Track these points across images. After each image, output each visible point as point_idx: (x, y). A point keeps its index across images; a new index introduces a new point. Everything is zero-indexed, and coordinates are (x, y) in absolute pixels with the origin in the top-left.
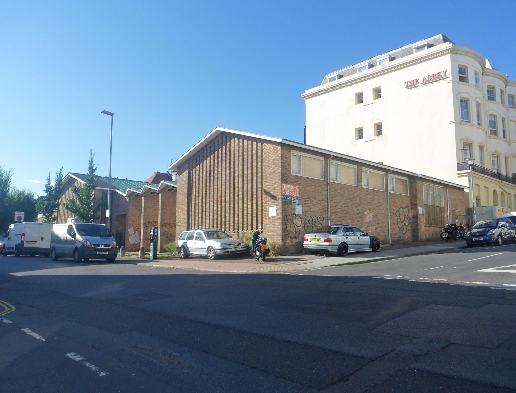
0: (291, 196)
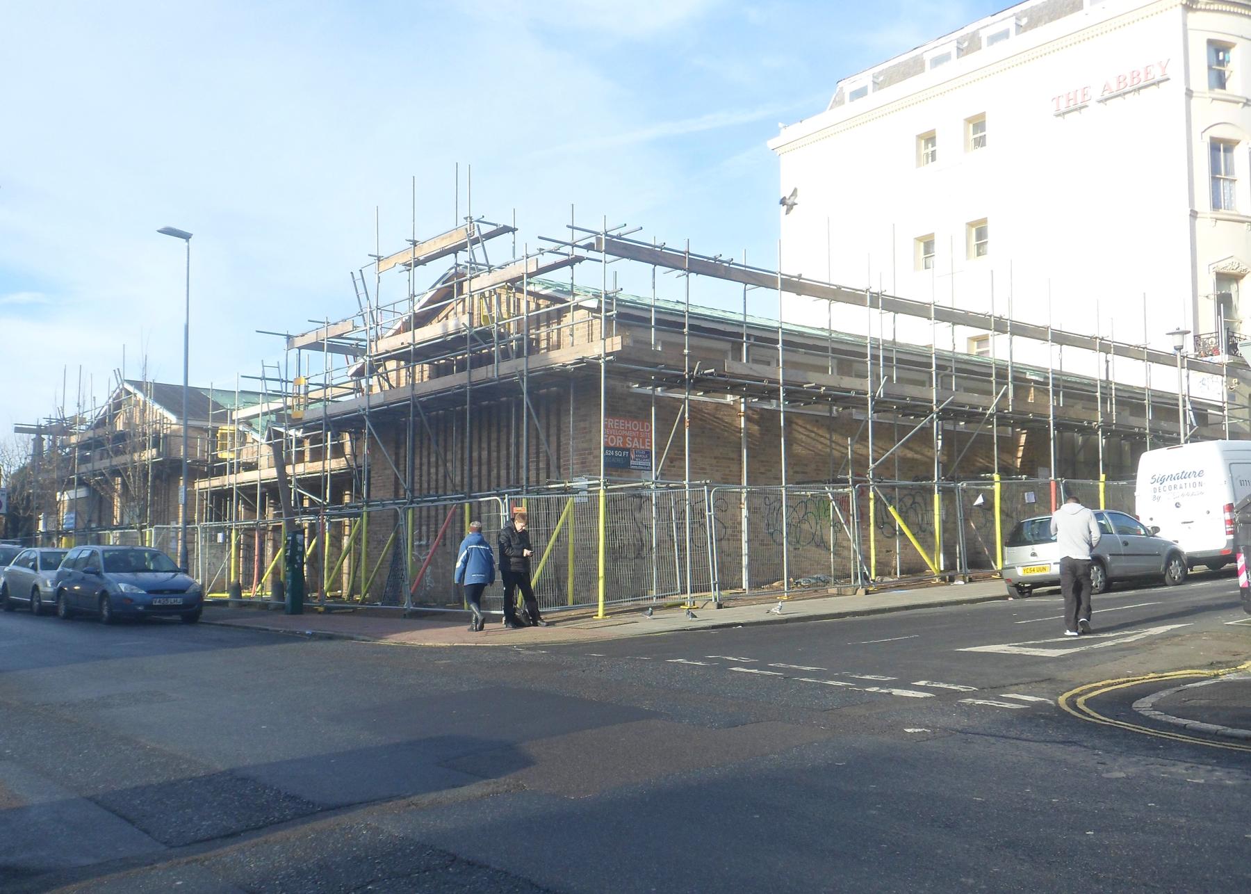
0: (628, 450)
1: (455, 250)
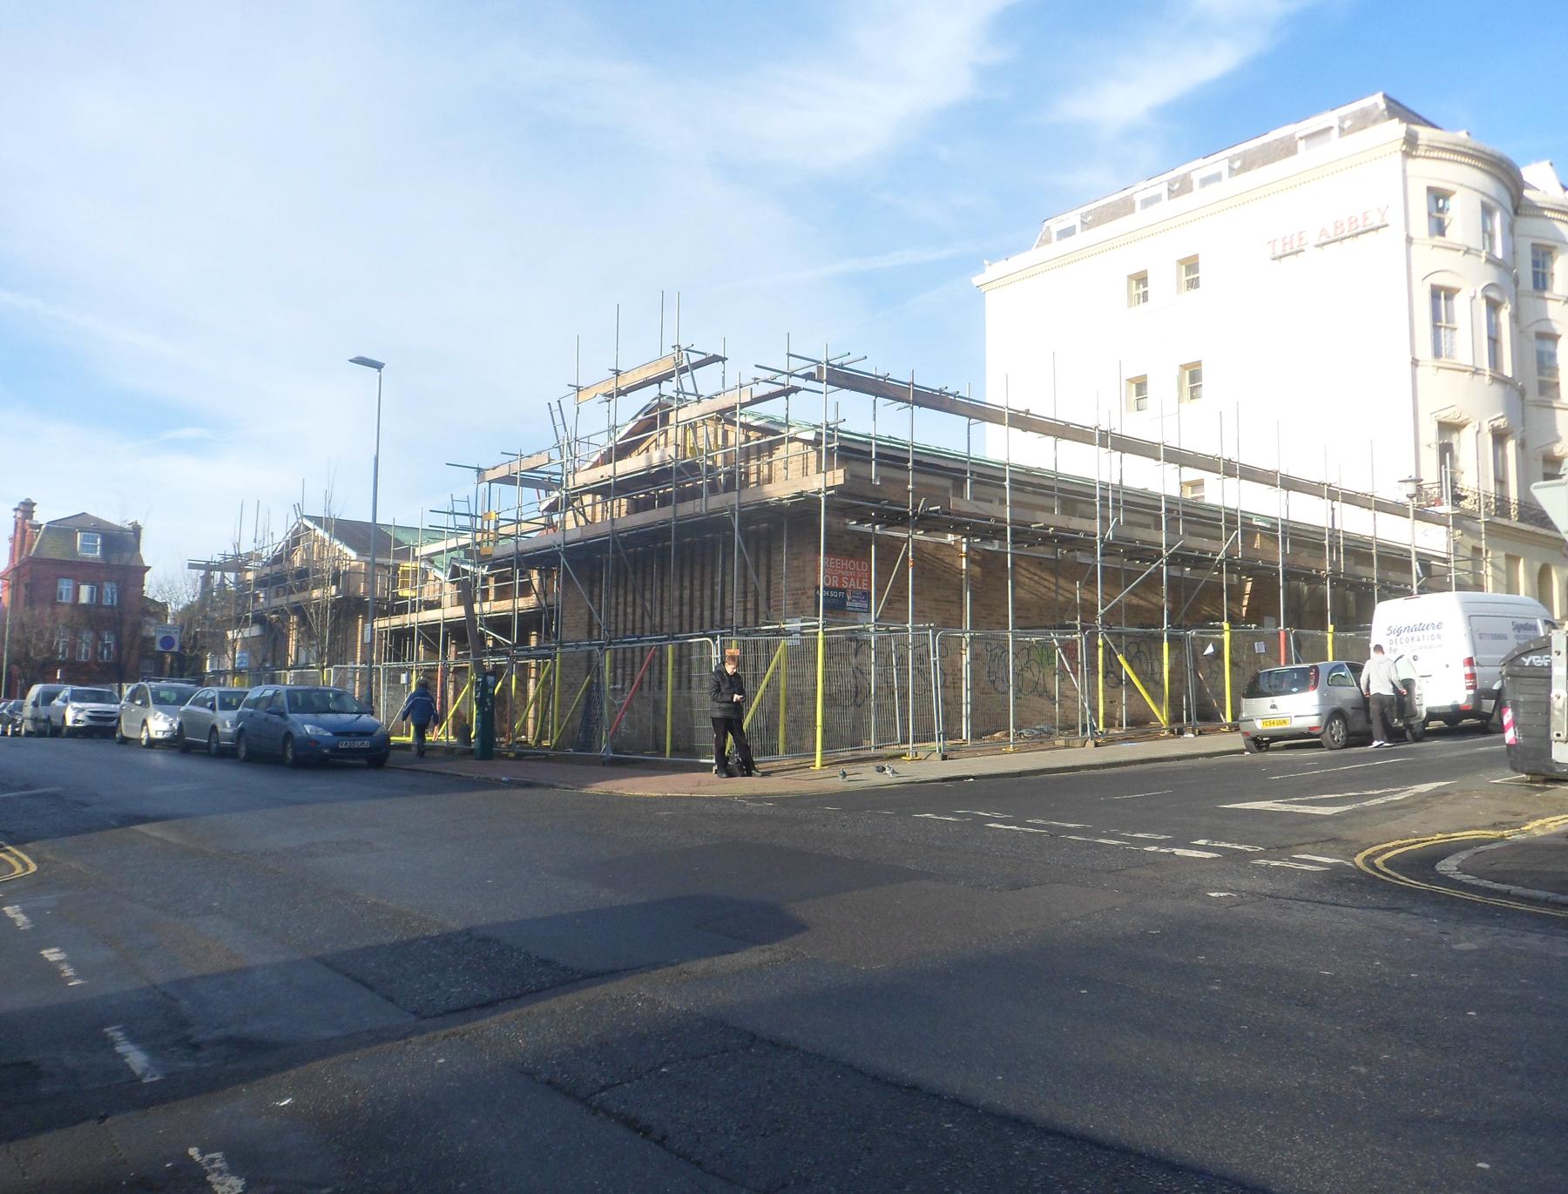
1: (658, 380)
